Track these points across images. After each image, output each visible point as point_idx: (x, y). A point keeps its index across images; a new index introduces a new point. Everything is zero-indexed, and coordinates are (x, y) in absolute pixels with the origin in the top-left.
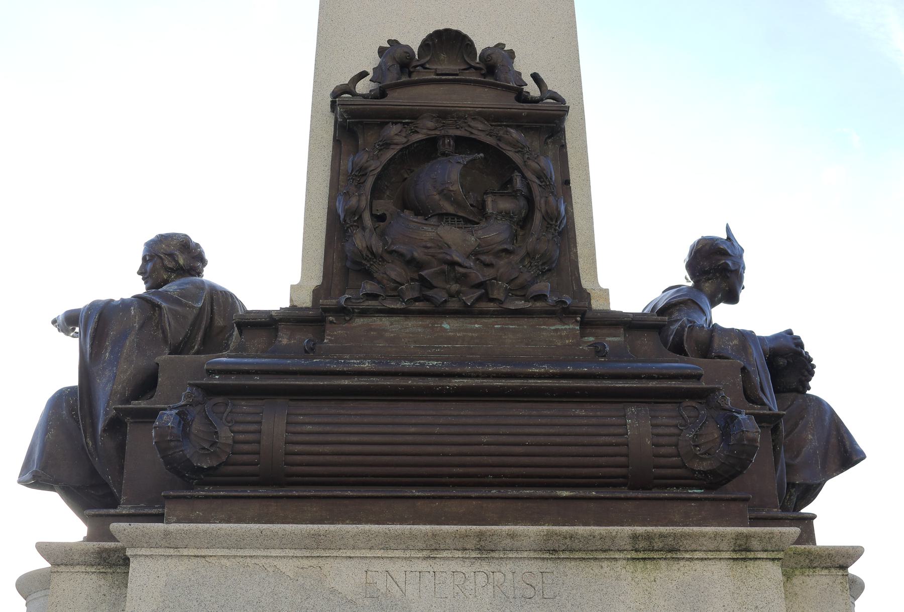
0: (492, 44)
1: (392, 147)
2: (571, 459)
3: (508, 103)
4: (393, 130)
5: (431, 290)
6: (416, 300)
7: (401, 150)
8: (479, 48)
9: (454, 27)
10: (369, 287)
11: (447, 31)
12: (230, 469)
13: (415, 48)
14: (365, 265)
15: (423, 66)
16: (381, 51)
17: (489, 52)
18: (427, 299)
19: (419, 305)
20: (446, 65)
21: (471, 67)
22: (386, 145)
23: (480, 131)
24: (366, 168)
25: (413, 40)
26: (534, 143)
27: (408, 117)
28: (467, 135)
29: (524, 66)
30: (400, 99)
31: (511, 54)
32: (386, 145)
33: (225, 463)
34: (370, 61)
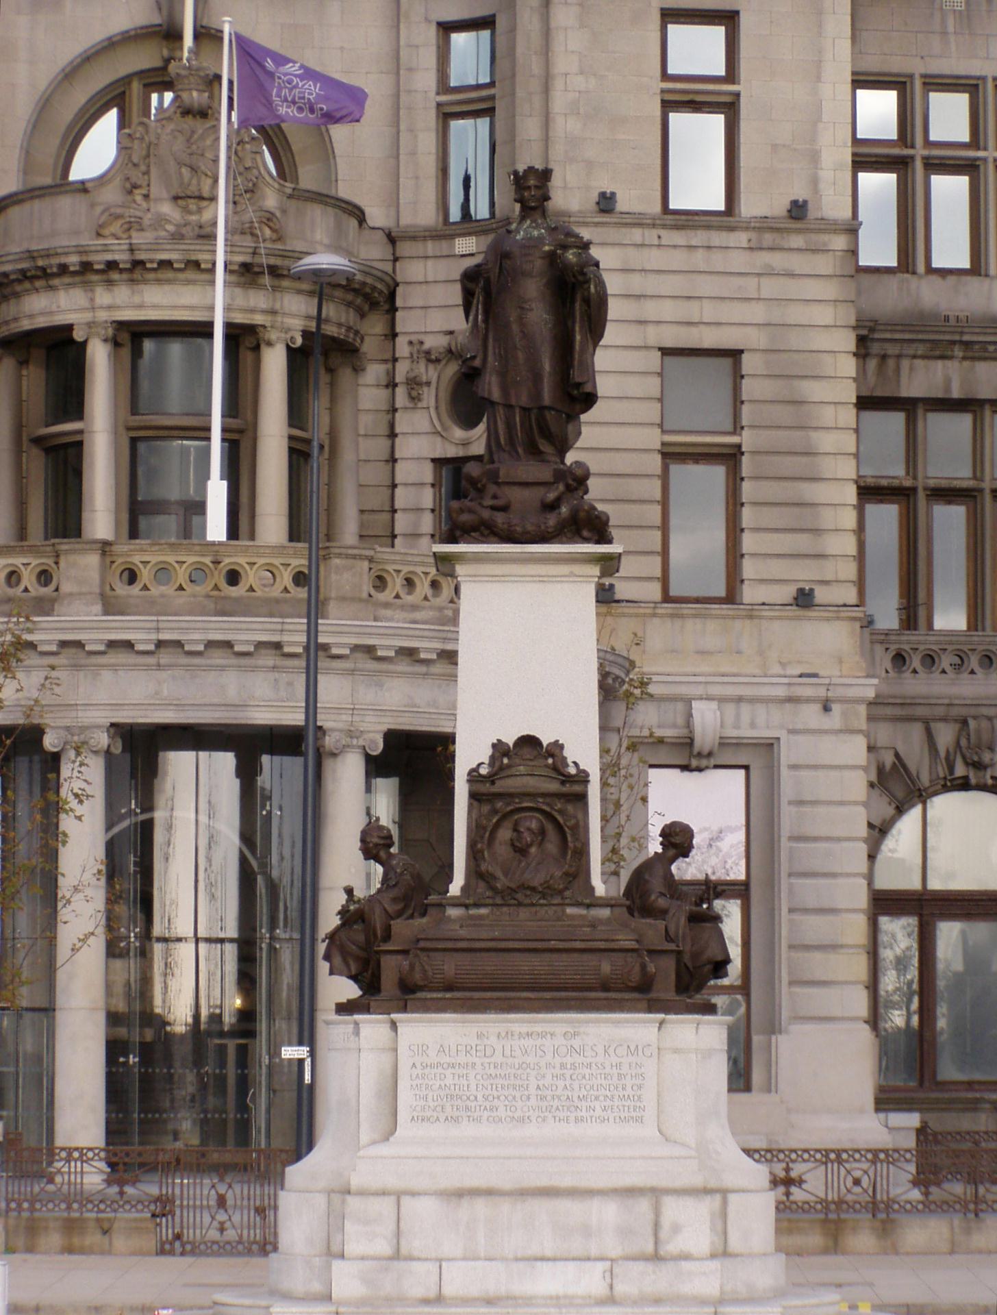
3: (554, 787)
4: (499, 805)
5: (510, 896)
8: (545, 744)
20: (527, 752)
22: (495, 812)
23: (541, 803)
25: (510, 740)
26: (570, 808)
29: (570, 754)
31: (562, 747)
34: (485, 754)
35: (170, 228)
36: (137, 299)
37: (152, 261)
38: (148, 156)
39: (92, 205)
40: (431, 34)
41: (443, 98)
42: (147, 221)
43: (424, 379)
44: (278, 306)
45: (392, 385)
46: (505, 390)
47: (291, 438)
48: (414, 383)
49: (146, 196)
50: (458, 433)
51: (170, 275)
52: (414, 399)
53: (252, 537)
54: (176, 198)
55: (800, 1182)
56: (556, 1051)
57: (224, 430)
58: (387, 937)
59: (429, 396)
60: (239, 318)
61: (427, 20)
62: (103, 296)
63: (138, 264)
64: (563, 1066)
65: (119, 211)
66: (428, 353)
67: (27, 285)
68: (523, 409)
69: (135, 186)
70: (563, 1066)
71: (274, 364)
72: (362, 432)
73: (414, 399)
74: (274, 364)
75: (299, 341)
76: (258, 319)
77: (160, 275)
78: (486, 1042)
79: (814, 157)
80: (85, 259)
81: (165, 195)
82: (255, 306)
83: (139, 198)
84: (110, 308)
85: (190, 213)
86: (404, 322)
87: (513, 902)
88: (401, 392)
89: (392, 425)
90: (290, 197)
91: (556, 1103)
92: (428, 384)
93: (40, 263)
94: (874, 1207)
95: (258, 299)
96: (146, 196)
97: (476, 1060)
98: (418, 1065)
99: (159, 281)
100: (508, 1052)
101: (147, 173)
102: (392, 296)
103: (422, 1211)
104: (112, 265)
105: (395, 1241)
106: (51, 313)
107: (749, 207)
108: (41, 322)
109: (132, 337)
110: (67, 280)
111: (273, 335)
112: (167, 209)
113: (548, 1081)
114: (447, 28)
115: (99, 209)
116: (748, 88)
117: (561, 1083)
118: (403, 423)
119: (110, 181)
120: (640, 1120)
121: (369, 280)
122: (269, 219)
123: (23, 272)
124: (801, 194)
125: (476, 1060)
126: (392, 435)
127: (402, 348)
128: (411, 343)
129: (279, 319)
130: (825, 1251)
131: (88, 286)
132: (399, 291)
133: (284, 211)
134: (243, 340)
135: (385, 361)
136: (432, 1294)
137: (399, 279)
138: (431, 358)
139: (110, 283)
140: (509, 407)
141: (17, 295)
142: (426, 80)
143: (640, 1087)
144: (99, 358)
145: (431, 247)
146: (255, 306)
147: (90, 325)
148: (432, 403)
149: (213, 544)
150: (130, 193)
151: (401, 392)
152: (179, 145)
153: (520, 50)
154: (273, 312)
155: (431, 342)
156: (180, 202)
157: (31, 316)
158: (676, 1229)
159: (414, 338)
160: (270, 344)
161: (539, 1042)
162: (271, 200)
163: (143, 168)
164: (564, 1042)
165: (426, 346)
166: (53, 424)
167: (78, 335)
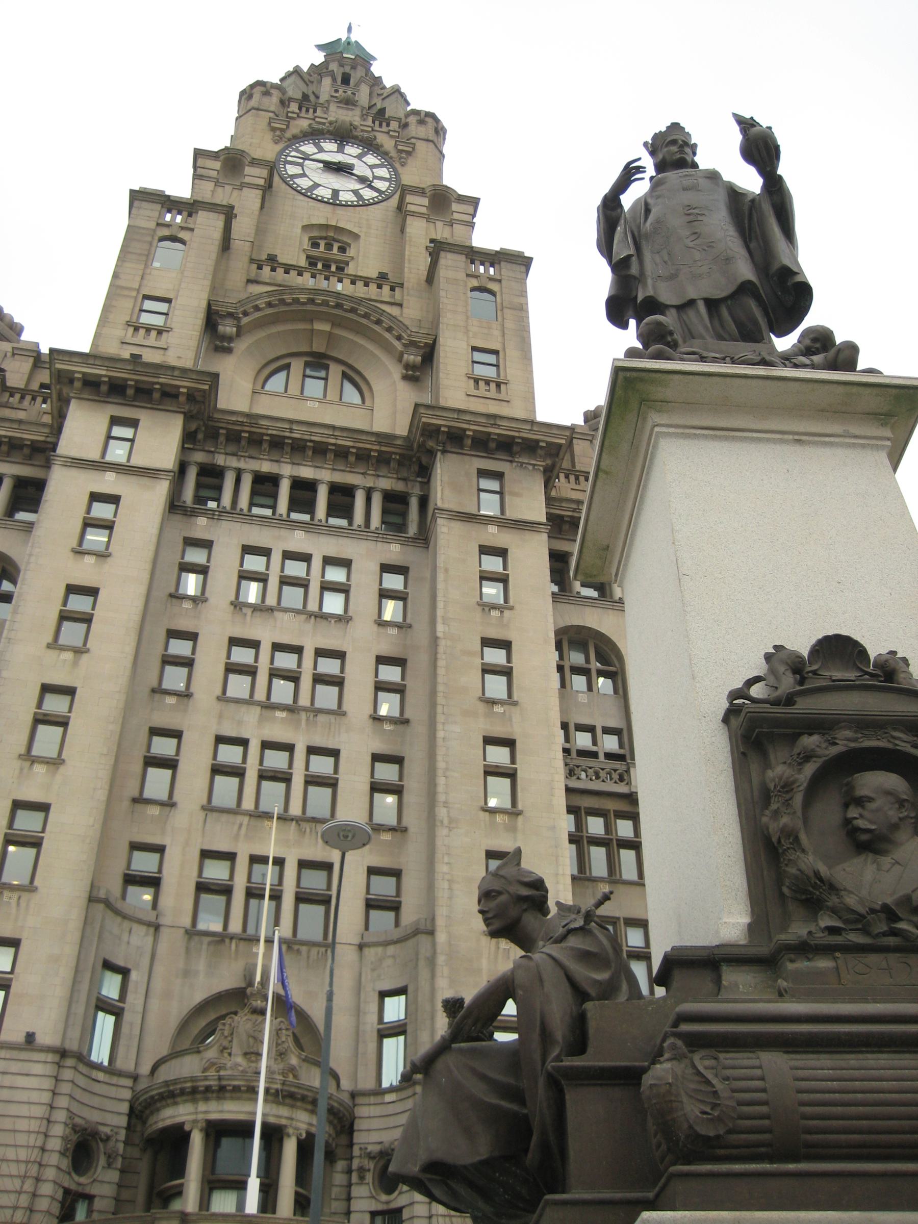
0: (884, 651)
1: (814, 759)
2: (903, 1109)
4: (810, 741)
6: (884, 934)
7: (825, 762)
8: (872, 654)
9: (830, 633)
10: (826, 921)
11: (838, 637)
12: (735, 1136)
13: (805, 653)
14: (811, 893)
15: (815, 673)
16: (768, 657)
17: (883, 658)
18: (894, 933)
19: (892, 941)
21: (867, 673)
24: (794, 782)
25: (802, 646)
27: (822, 725)
28: (890, 746)
30: (806, 706)
32: (807, 757)
33: (730, 1132)
35: (241, 1068)
36: (220, 1108)
37: (229, 1085)
38: (232, 1034)
39: (202, 1059)
40: (376, 997)
41: (381, 1026)
42: (229, 1065)
43: (367, 1167)
44: (294, 1116)
45: (349, 1171)
47: (297, 1193)
48: (362, 1170)
49: (230, 1054)
50: (384, 1197)
51: (238, 1095)
52: (362, 1178)
53: (274, 1212)
54: (245, 1054)
57: (259, 1081)
58: (579, 1045)
59: (369, 1177)
60: (272, 1120)
61: (374, 990)
62: (202, 1106)
63: (222, 1089)
65: (215, 1060)
66: (370, 1153)
67: (164, 1103)
69: (225, 1048)
71: (290, 1150)
72: (333, 1197)
73: (362, 1178)
74: (290, 1150)
75: (304, 1135)
76: (284, 1122)
77: (234, 1095)
80: (195, 1084)
81: (239, 1052)
82: (281, 1114)
83: (226, 1055)
84: (206, 1112)
85: (252, 1062)
86: (358, 1138)
87: (892, 941)
88: (355, 1177)
89: (349, 1193)
90: (304, 1060)
92: (369, 1170)
93: (171, 1088)
95: (284, 1111)
96: (230, 1054)
99: (232, 1098)
101: (231, 1041)
102: (352, 1124)
104: (208, 1089)
106: (174, 1117)
108: (169, 1122)
109: (218, 1132)
110: (184, 1098)
111: (290, 1131)
112: (239, 1059)
114: (383, 995)
115: (205, 1061)
118: (356, 1191)
119: (212, 1047)
121: (342, 1109)
122: (292, 1069)
123: (160, 1094)
126: (349, 1199)
127: (356, 1151)
128: (361, 1149)
129: (294, 1123)
131: (195, 1101)
132: (356, 1121)
133: (300, 1067)
134: (273, 1136)
135: (346, 1159)
137: (356, 1115)
138: (370, 1156)
139: (207, 1099)
141: (158, 1110)
142: (373, 1018)
144: (197, 1141)
145: (372, 1099)
146: (281, 1114)
147: (195, 1121)
148: (371, 1181)
149: (248, 1216)
150: (222, 1051)
151: (355, 1177)
152: (249, 1025)
153: (420, 999)
154: (291, 1119)
155: (370, 1148)
156: (248, 1056)
157: (163, 1120)
159: (362, 1146)
160: (289, 1136)
162: (294, 1061)
163: (230, 1038)
165: (369, 1150)
166: (172, 1181)
167: (187, 1128)
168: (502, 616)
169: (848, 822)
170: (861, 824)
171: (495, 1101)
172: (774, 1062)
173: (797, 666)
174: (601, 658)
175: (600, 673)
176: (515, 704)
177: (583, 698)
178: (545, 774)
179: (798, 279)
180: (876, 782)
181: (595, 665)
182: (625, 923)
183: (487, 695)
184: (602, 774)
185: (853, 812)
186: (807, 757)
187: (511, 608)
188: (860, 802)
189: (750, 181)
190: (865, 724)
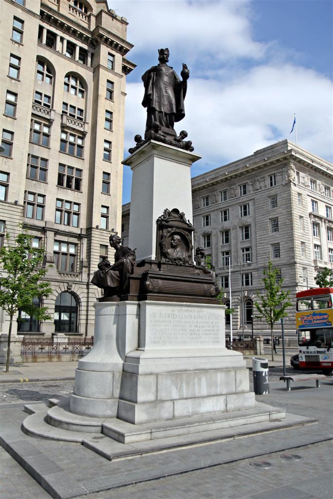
4: (170, 229)
27: (171, 227)
46: (160, 107)
55: (68, 348)
56: (195, 317)
58: (132, 273)
64: (197, 322)
68: (166, 114)
70: (197, 322)
78: (175, 313)
79: (19, 195)
91: (195, 336)
94: (56, 353)
97: (171, 319)
98: (153, 321)
100: (181, 317)
103: (166, 382)
105: (156, 394)
107: (9, 200)
113: (193, 328)
116: (10, 184)
117: (197, 329)
120: (218, 342)
124: (17, 200)
125: (171, 319)
130: (48, 361)
136: (171, 416)
140: (160, 112)
143: (218, 330)
158: (241, 382)
161: (190, 313)
164: (197, 314)
168: (19, 47)
169: (171, 243)
170: (174, 244)
171: (117, 278)
172: (160, 282)
173: (169, 214)
174: (48, 70)
175: (47, 76)
176: (19, 81)
177: (40, 82)
178: (25, 108)
179: (183, 112)
180: (177, 237)
181: (46, 72)
182: (32, 157)
183: (10, 75)
184: (42, 110)
185: (172, 241)
186: (169, 232)
187: (23, 45)
188: (174, 240)
189: (181, 79)
190: (178, 228)
